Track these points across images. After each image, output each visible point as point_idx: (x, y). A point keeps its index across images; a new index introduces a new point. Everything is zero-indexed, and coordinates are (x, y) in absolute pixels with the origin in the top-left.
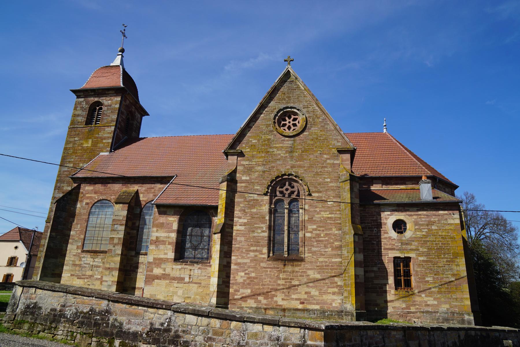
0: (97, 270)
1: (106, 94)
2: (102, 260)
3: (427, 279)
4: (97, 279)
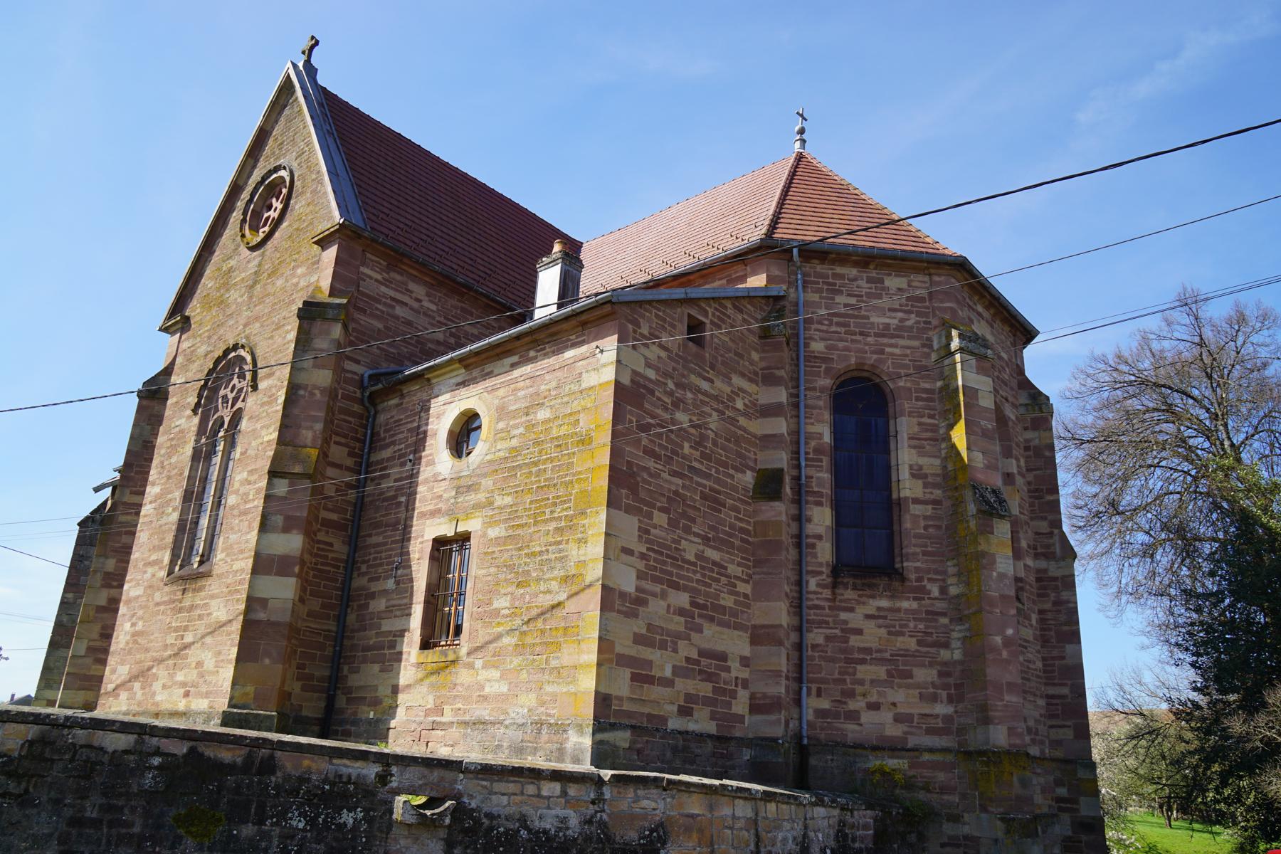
3: (496, 605)
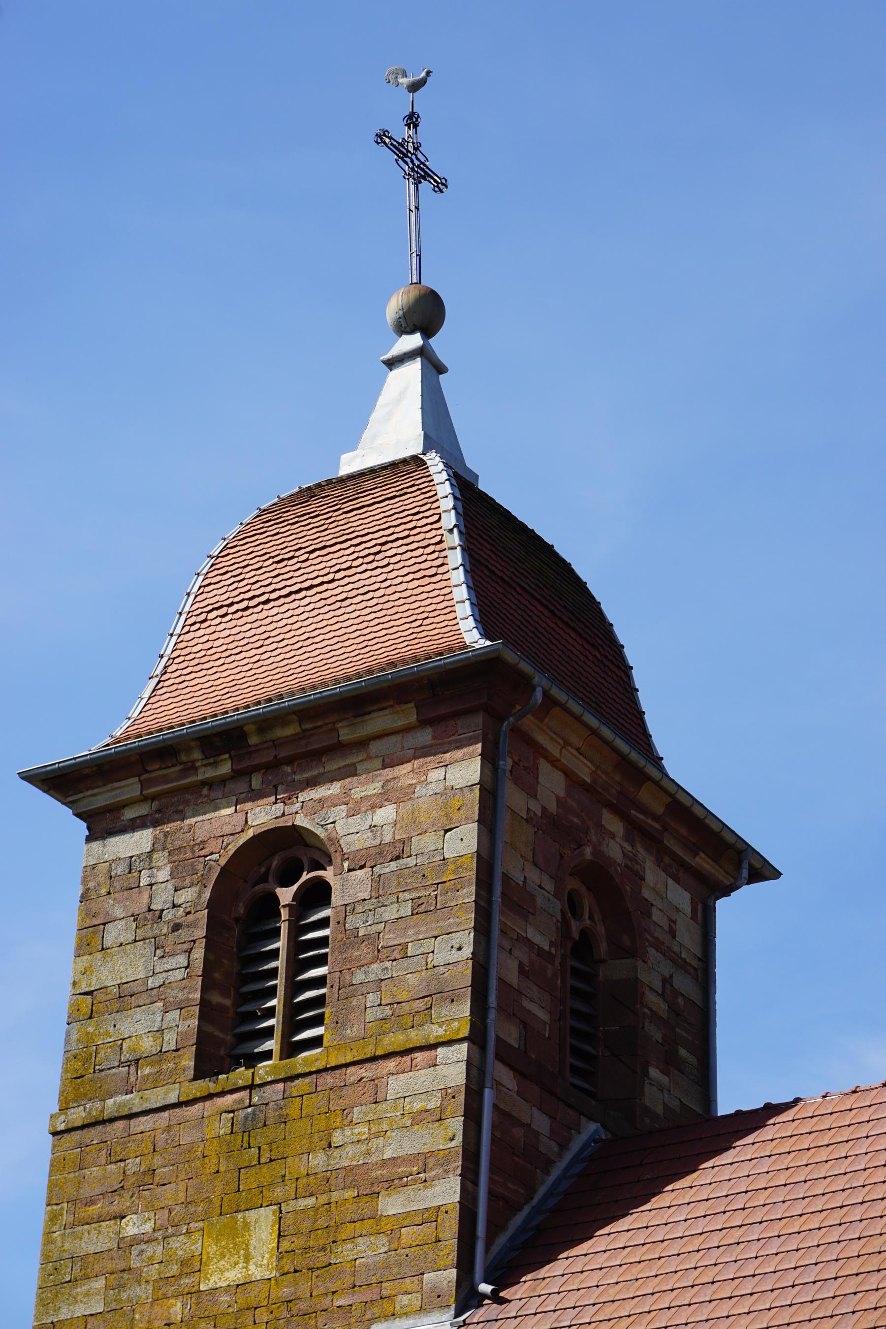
1: (339, 748)
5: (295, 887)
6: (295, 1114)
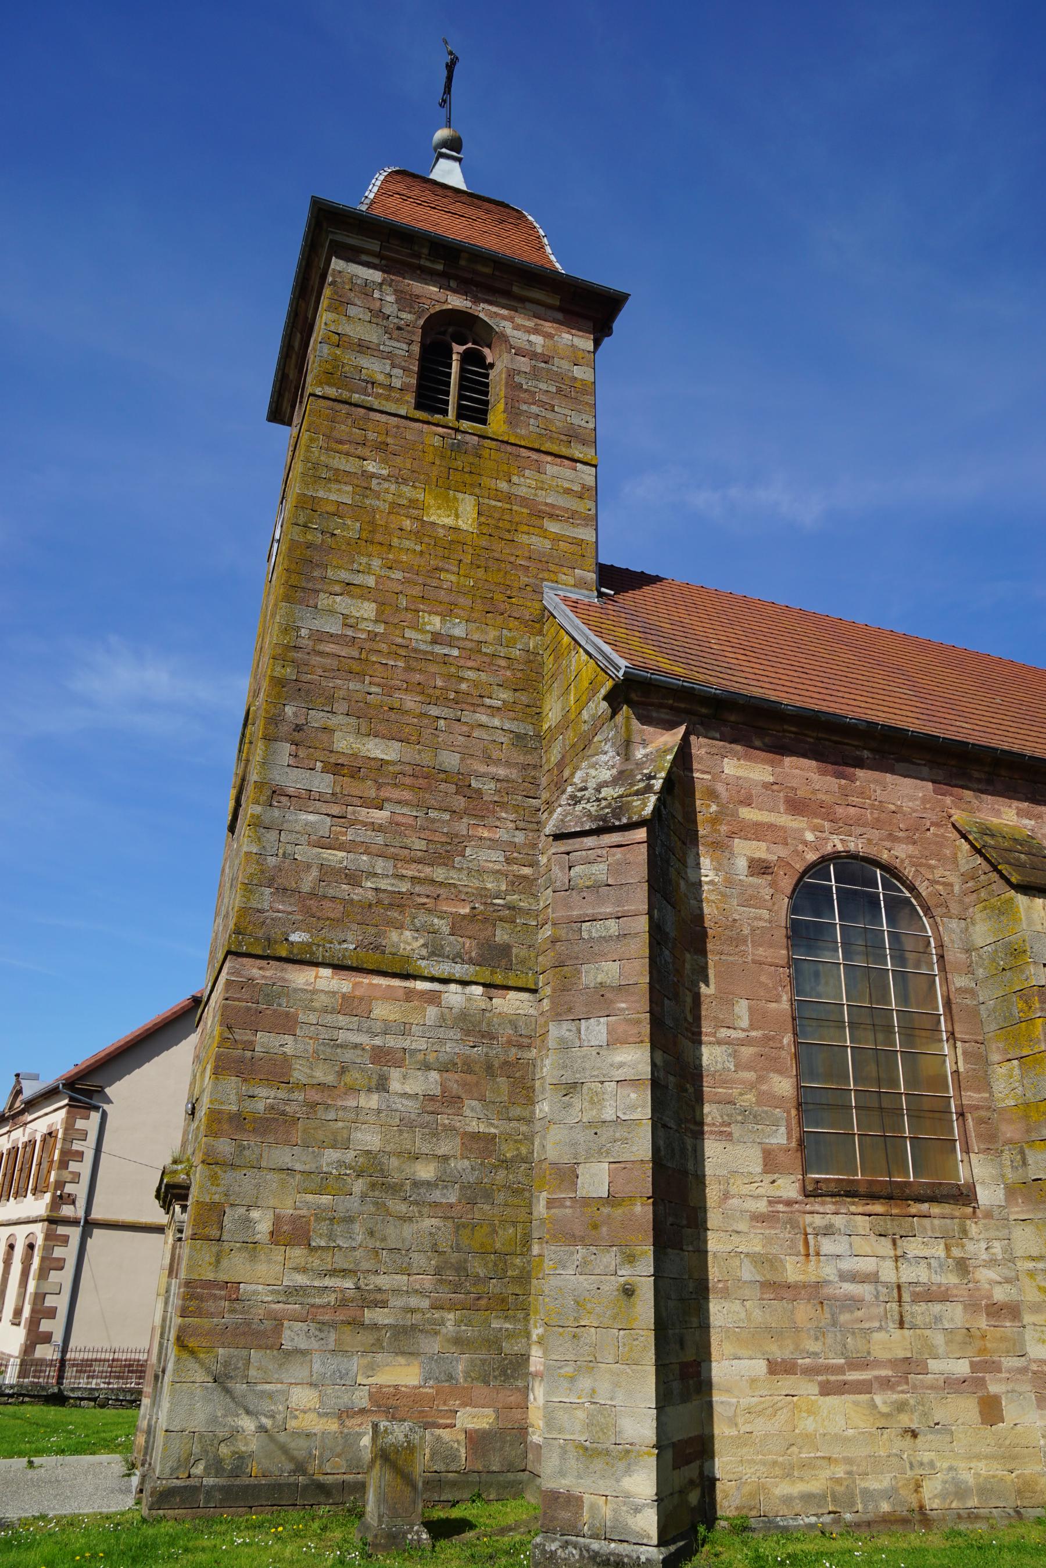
0: (938, 1319)
1: (508, 294)
2: (947, 1248)
4: (953, 1385)
5: (465, 347)
6: (487, 456)
